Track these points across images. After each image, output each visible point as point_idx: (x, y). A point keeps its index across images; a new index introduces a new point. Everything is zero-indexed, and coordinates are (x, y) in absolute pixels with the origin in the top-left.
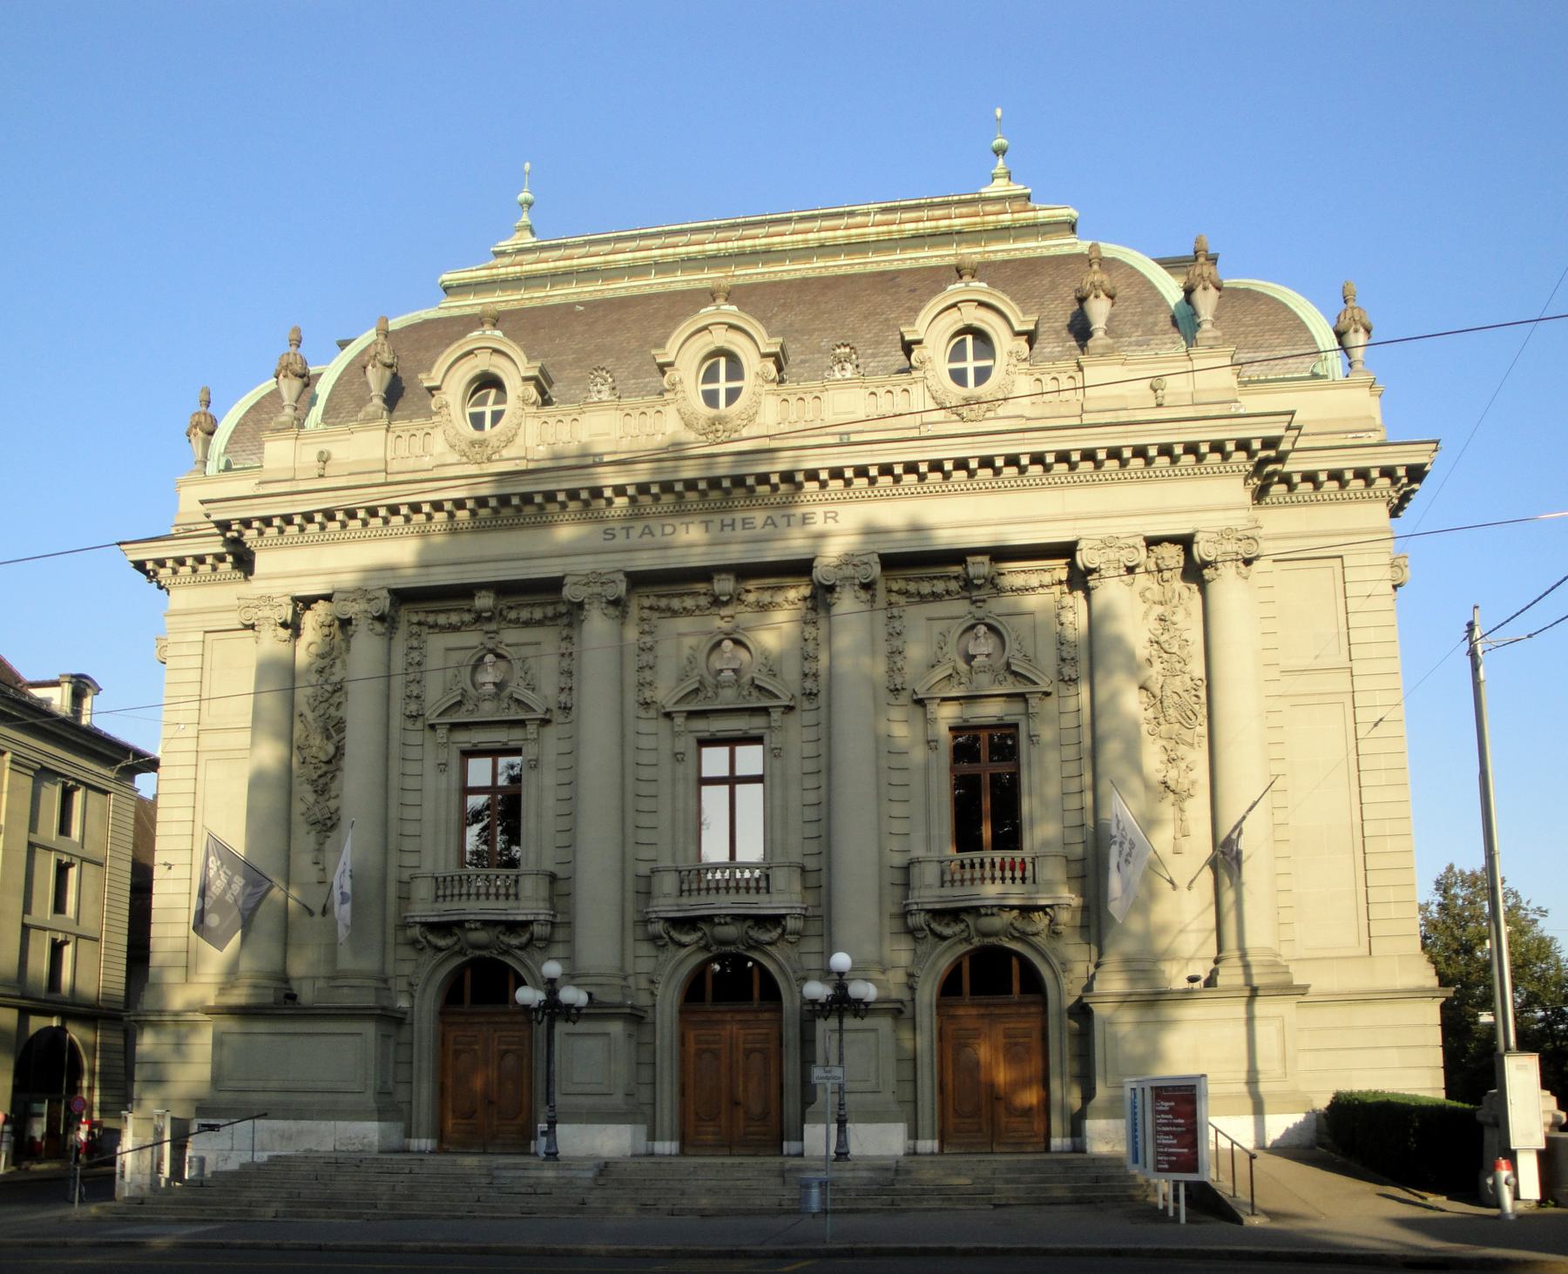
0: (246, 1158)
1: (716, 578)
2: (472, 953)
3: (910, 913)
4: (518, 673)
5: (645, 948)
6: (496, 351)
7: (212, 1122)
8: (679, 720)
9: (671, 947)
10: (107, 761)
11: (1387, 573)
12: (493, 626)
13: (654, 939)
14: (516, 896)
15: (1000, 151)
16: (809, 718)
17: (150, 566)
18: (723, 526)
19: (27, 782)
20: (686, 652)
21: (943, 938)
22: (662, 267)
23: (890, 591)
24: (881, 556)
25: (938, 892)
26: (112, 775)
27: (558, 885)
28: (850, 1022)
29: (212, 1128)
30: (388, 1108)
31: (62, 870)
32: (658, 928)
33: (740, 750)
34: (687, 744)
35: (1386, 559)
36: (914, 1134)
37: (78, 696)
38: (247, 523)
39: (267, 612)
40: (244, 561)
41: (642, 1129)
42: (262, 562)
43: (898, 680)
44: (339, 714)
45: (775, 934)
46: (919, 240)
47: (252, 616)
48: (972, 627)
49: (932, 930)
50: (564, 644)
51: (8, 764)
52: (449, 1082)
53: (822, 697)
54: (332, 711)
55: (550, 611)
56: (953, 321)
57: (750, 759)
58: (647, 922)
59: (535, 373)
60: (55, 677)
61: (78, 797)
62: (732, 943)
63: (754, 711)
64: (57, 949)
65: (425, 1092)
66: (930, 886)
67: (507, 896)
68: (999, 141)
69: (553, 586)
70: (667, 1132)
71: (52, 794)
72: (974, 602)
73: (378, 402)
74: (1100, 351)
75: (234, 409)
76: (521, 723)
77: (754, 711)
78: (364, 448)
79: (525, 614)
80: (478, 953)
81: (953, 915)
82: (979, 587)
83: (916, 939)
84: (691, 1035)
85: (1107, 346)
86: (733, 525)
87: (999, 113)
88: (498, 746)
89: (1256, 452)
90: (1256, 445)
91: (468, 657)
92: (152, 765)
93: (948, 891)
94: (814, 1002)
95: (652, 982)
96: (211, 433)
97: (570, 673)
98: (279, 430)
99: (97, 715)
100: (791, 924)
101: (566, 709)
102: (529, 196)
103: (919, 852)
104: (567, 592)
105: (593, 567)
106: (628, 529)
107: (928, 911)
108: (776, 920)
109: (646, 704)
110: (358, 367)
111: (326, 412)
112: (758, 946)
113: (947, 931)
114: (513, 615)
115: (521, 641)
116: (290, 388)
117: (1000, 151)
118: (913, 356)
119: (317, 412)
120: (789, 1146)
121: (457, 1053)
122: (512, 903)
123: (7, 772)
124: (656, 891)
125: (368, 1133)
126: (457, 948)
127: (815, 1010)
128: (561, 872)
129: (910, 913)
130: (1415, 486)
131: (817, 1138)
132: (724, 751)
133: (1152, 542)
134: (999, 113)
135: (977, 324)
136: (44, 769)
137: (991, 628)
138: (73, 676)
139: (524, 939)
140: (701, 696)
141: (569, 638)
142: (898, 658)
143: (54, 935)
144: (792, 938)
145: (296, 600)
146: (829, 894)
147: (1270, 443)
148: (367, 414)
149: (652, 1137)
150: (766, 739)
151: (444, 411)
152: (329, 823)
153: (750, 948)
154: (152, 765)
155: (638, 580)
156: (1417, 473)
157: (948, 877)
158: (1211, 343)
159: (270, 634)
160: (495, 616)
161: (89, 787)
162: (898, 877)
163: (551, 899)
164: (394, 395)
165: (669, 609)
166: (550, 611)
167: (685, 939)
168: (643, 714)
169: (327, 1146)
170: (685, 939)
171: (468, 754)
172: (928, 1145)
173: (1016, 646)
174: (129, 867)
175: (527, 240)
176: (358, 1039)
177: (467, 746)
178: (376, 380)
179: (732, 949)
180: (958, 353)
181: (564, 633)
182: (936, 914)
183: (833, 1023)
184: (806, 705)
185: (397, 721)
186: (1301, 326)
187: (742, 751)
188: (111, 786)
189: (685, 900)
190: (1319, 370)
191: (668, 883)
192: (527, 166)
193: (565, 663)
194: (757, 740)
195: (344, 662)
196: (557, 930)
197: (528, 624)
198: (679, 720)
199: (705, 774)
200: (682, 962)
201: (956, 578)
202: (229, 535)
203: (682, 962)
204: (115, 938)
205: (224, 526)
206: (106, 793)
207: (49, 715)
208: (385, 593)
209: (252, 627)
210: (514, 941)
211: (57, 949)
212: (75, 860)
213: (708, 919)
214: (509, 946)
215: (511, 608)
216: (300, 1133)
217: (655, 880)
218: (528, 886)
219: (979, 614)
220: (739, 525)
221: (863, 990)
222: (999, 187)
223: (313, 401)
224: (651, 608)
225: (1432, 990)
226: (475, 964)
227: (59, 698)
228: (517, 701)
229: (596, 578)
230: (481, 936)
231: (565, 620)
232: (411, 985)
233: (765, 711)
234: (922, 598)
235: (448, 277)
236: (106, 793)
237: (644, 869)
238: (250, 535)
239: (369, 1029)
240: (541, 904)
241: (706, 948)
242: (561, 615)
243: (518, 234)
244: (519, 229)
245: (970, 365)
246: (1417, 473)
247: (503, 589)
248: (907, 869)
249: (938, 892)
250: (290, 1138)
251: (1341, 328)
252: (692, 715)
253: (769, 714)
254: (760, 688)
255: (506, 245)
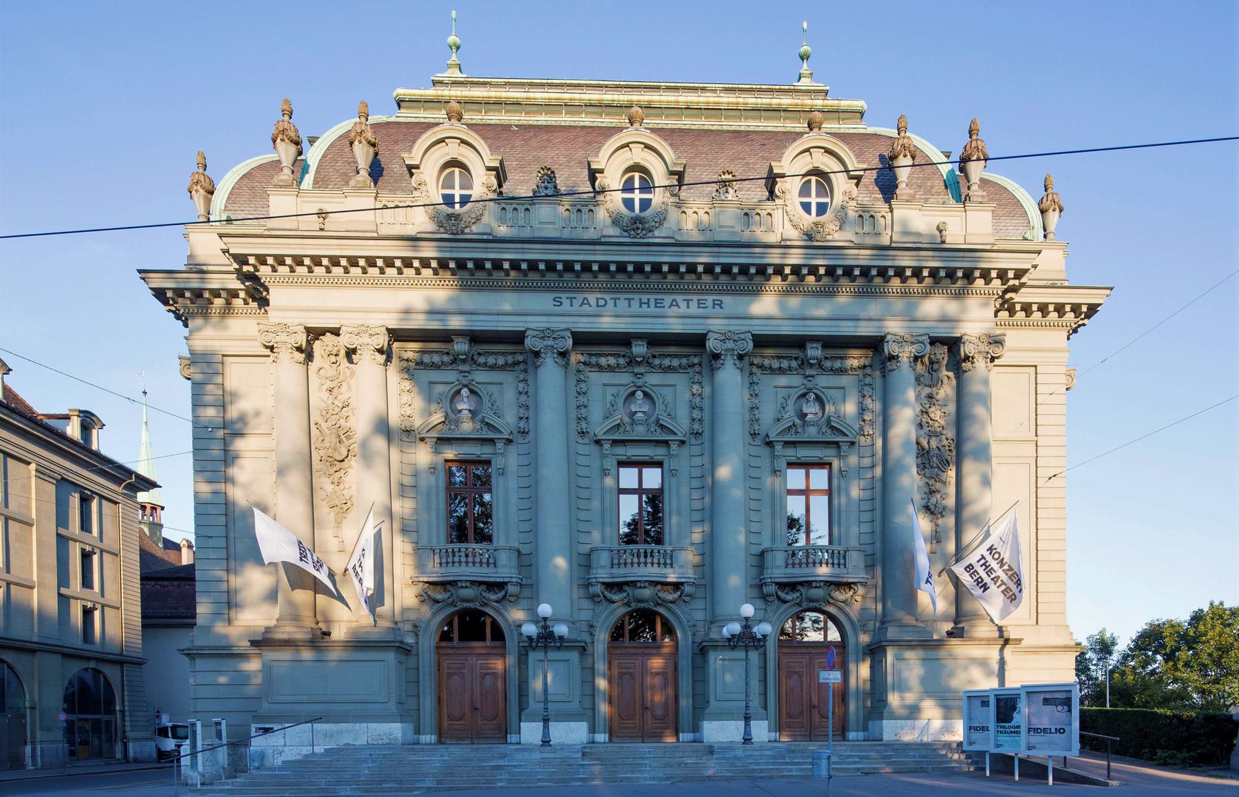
0: (306, 750)
1: (809, 345)
2: (460, 605)
3: (766, 584)
4: (486, 404)
5: (586, 604)
6: (463, 142)
7: (267, 726)
8: (607, 446)
9: (604, 602)
10: (118, 481)
11: (1063, 379)
12: (467, 368)
13: (592, 597)
14: (495, 564)
15: (804, 57)
16: (696, 450)
17: (169, 294)
18: (641, 303)
19: (51, 489)
20: (610, 398)
21: (785, 602)
22: (569, 107)
23: (752, 364)
24: (572, 333)
25: (783, 571)
26: (120, 489)
27: (527, 561)
28: (552, 655)
29: (267, 731)
30: (408, 713)
31: (86, 557)
32: (598, 589)
33: (645, 470)
34: (610, 463)
35: (1063, 370)
36: (592, 730)
37: (86, 428)
38: (262, 259)
39: (283, 337)
40: (258, 295)
41: (410, 727)
42: (276, 296)
43: (584, 425)
44: (348, 425)
45: (500, 595)
46: (757, 111)
47: (272, 339)
48: (804, 395)
49: (778, 597)
50: (521, 385)
51: (33, 473)
52: (444, 695)
53: (706, 435)
54: (342, 422)
55: (510, 359)
56: (805, 164)
57: (819, 478)
58: (588, 585)
59: (497, 164)
60: (66, 412)
61: (94, 505)
62: (647, 601)
63: (484, 441)
64: (88, 613)
65: (428, 703)
66: (779, 567)
67: (488, 564)
68: (805, 48)
69: (517, 338)
70: (602, 728)
71: (75, 500)
72: (807, 377)
73: (364, 173)
74: (905, 197)
75: (229, 174)
76: (666, 443)
77: (484, 441)
78: (359, 213)
79: (491, 360)
80: (466, 605)
81: (792, 586)
82: (811, 365)
83: (766, 601)
84: (444, 664)
85: (910, 195)
86: (648, 303)
87: (805, 25)
88: (473, 457)
89: (1008, 280)
90: (1011, 274)
91: (624, 392)
92: (150, 485)
93: (790, 570)
94: (530, 638)
95: (592, 626)
96: (212, 193)
97: (527, 407)
98: (281, 187)
99: (103, 442)
100: (511, 589)
101: (524, 433)
102: (458, 41)
103: (766, 544)
104: (528, 342)
105: (547, 325)
106: (571, 299)
107: (776, 583)
108: (501, 586)
109: (582, 433)
110: (348, 140)
111: (316, 182)
112: (663, 602)
113: (789, 597)
114: (482, 360)
115: (488, 380)
116: (285, 152)
117: (804, 57)
118: (597, 183)
119: (309, 180)
120: (512, 738)
121: (450, 676)
122: (492, 569)
123: (33, 479)
124: (594, 565)
125: (395, 730)
126: (450, 601)
127: (531, 644)
128: (524, 549)
129: (766, 584)
130: (1086, 321)
131: (530, 732)
132: (801, 472)
133: (934, 341)
134: (805, 25)
135: (643, 163)
136: (63, 479)
137: (818, 399)
138: (80, 411)
139: (500, 595)
140: (622, 430)
141: (525, 380)
142: (756, 412)
143: (85, 603)
144: (687, 599)
145: (309, 330)
146: (712, 570)
147: (1020, 274)
148: (358, 182)
149: (418, 731)
150: (666, 464)
151: (423, 188)
152: (345, 507)
153: (658, 604)
154: (150, 485)
155: (582, 340)
156: (1093, 309)
157: (616, 561)
158: (980, 199)
159: (288, 356)
160: (471, 359)
161: (102, 497)
162: (754, 561)
163: (520, 566)
164: (376, 171)
165: (598, 365)
166: (510, 359)
167: (615, 598)
168: (580, 441)
169: (362, 741)
170: (615, 598)
171: (622, 464)
172: (601, 737)
173: (663, 407)
174: (138, 558)
175: (456, 74)
176: (380, 664)
177: (793, 459)
178: (362, 155)
179: (471, 605)
180: (805, 191)
181: (522, 377)
182: (781, 586)
183: (540, 655)
184: (693, 441)
185: (574, 435)
186: (1018, 203)
187: (814, 473)
188: (119, 498)
189: (615, 570)
190: (1027, 236)
191: (780, 558)
192: (454, 13)
193: (523, 398)
194: (659, 464)
195: (349, 385)
196: (528, 586)
197: (494, 368)
198: (607, 446)
199: (621, 486)
200: (612, 612)
201: (796, 358)
202: (245, 268)
203: (612, 612)
204: (131, 608)
205: (241, 259)
206: (116, 503)
207: (63, 437)
208: (384, 329)
209: (272, 348)
210: (493, 597)
211: (88, 613)
212: (97, 551)
213: (633, 584)
214: (490, 600)
215: (480, 354)
216: (339, 732)
217: (594, 556)
218: (504, 558)
219: (810, 385)
220: (652, 303)
221: (561, 629)
222: (805, 83)
223: (305, 170)
224: (584, 363)
225: (994, 639)
226: (462, 614)
227: (73, 430)
228: (487, 424)
229: (544, 334)
230: (469, 592)
231: (522, 367)
232: (416, 626)
233: (666, 443)
234: (601, 369)
235: (401, 92)
236: (116, 503)
237: (585, 549)
238: (264, 271)
239: (390, 657)
240: (513, 571)
241: (628, 604)
242: (519, 363)
243: (450, 70)
244: (449, 66)
245: (814, 200)
246: (1093, 309)
247: (475, 337)
248: (762, 554)
249: (783, 571)
250: (332, 736)
251: (1044, 206)
252: (615, 442)
253: (669, 446)
254: (662, 426)
255: (439, 76)
